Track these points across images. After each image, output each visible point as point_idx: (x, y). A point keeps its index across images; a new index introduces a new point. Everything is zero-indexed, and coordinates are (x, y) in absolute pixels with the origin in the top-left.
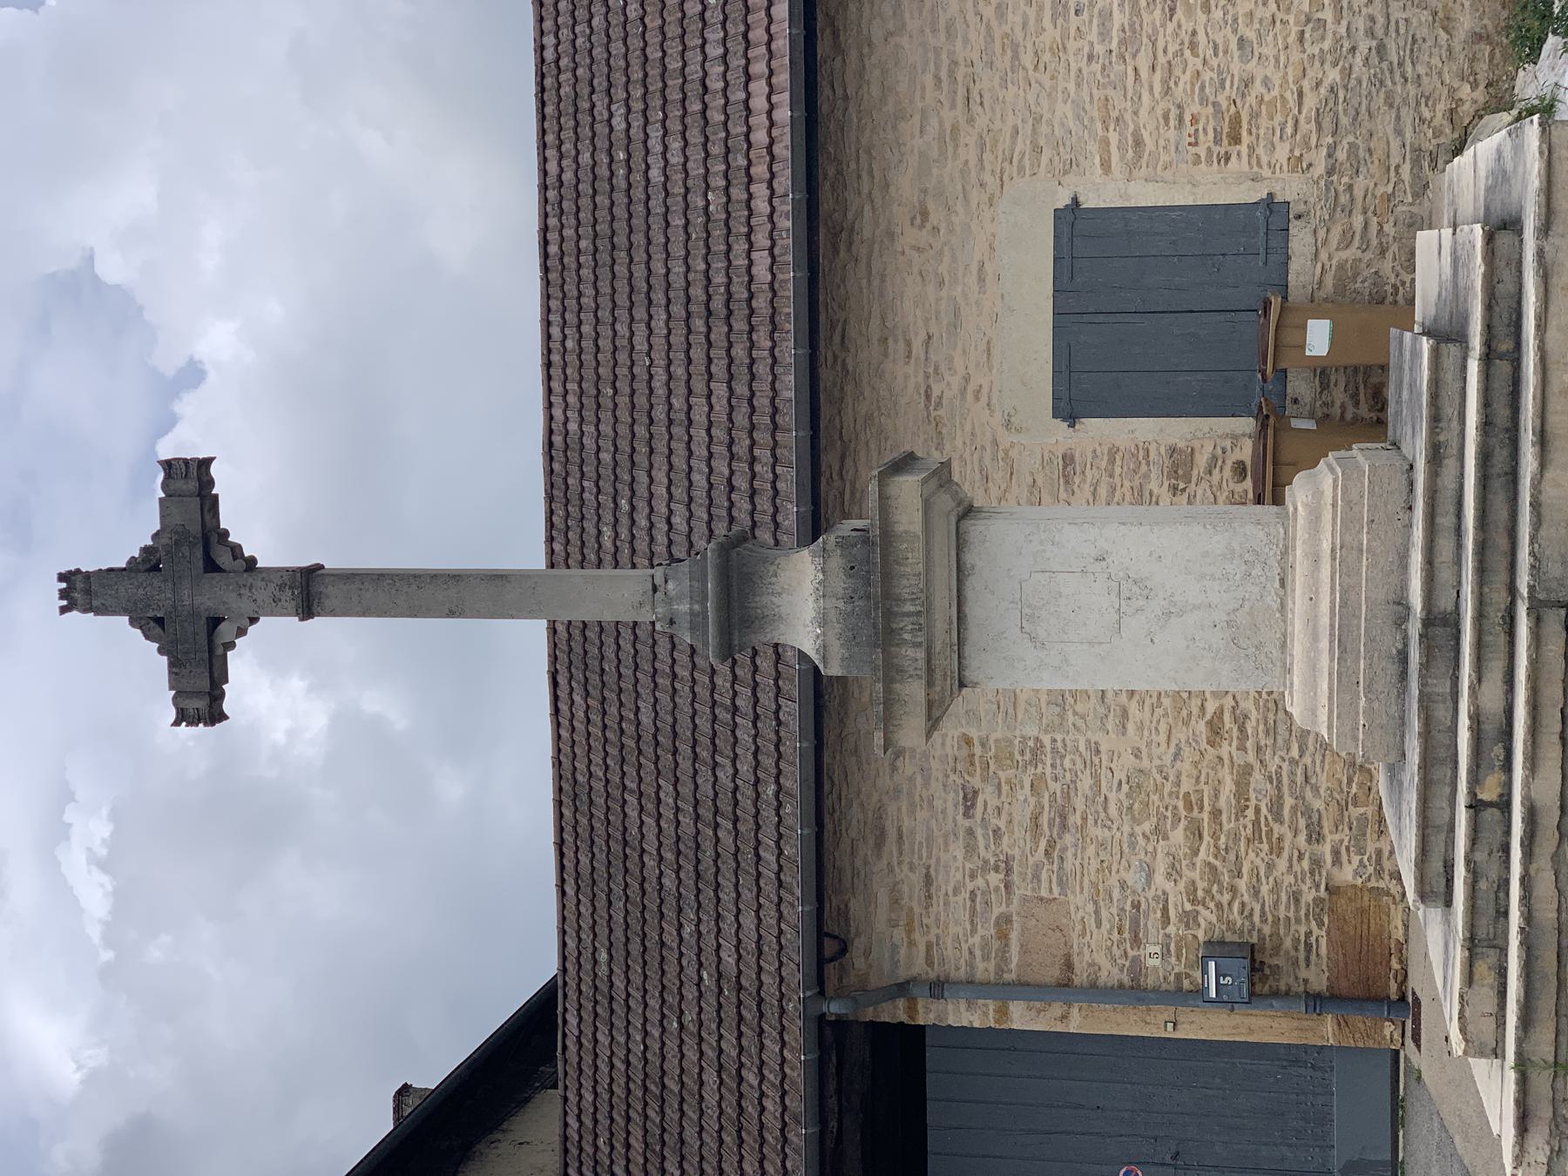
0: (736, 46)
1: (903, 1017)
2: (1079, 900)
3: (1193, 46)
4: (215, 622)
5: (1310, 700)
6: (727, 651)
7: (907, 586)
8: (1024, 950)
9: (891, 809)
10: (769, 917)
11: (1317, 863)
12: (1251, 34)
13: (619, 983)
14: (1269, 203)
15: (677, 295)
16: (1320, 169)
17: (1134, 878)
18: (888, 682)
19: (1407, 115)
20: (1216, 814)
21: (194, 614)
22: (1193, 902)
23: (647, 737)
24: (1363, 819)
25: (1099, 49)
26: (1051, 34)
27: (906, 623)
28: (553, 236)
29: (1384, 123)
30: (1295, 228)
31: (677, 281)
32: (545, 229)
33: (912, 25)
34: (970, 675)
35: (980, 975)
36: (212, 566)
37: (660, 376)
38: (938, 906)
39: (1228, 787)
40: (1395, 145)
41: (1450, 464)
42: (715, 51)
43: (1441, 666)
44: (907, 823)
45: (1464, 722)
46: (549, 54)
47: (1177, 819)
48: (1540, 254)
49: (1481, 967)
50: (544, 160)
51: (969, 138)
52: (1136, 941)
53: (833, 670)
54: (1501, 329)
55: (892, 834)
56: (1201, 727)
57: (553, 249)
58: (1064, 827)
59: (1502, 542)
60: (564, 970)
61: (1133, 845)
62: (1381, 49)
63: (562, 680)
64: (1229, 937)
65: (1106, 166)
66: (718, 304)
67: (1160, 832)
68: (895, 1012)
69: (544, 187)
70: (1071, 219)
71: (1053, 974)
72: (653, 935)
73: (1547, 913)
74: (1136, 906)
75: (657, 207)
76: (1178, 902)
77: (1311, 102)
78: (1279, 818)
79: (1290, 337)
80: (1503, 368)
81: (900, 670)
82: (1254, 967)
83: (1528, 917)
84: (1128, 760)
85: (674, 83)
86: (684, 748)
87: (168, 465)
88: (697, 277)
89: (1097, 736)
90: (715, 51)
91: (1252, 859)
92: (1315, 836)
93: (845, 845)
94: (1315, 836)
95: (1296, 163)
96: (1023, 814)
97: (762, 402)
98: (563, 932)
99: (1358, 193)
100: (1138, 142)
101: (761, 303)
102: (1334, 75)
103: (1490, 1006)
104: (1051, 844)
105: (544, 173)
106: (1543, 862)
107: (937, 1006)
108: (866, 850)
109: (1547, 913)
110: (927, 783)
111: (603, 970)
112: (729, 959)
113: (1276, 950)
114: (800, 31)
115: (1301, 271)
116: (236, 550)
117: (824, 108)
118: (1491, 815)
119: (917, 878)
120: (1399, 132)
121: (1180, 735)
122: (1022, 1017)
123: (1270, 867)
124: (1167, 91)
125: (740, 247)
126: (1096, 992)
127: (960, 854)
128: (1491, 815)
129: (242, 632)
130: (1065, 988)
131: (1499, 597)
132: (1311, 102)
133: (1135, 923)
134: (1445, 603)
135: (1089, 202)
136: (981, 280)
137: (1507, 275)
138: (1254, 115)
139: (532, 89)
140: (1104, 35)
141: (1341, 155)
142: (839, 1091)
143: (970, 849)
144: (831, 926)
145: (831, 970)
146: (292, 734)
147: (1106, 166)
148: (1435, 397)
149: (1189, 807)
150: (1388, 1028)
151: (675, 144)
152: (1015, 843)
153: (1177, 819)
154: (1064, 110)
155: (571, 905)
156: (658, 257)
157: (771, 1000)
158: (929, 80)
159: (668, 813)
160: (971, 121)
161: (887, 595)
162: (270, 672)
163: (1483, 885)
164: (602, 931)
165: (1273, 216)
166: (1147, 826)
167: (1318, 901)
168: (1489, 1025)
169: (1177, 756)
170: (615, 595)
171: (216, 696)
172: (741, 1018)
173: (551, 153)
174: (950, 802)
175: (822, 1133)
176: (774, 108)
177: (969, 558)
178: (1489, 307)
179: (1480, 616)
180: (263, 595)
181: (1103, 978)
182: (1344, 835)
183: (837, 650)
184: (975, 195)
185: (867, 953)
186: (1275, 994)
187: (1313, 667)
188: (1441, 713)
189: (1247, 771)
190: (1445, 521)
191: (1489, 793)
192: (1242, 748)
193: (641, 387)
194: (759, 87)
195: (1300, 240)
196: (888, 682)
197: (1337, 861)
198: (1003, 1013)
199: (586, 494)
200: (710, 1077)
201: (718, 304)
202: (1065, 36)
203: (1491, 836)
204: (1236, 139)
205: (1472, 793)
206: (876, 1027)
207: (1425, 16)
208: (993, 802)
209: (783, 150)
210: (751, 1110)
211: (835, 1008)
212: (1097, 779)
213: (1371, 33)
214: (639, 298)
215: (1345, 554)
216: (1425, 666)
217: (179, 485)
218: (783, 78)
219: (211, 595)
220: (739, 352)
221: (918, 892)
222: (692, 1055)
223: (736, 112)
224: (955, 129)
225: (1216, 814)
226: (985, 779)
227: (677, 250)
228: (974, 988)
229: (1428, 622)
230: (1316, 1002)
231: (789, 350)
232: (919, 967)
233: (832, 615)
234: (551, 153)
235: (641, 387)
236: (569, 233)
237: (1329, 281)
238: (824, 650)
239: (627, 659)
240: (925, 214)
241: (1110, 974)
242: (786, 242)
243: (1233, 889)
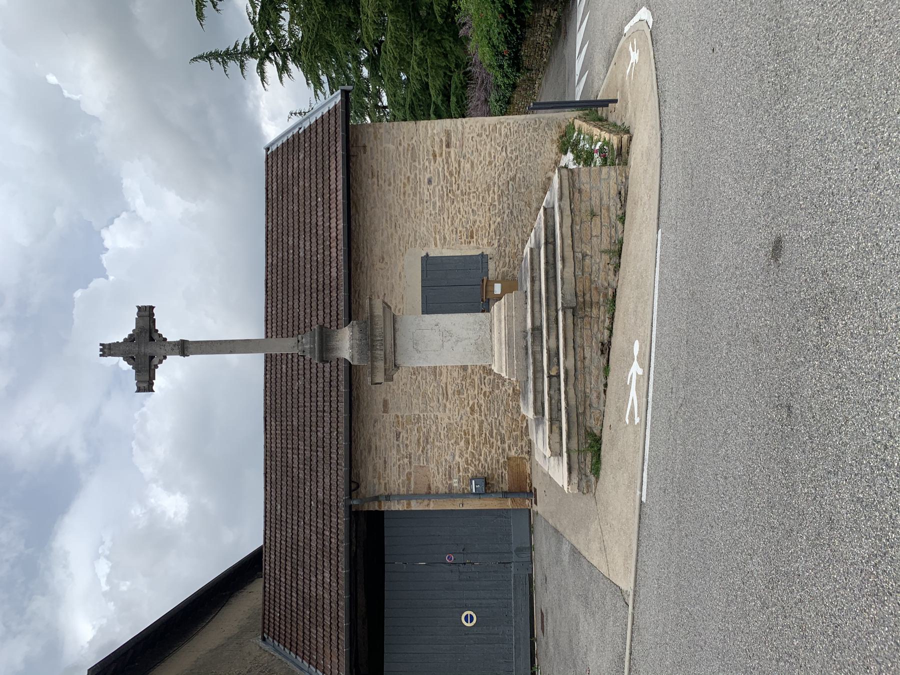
0: (326, 211)
1: (377, 508)
2: (432, 466)
3: (459, 212)
4: (152, 358)
5: (500, 366)
6: (323, 360)
7: (378, 331)
8: (415, 483)
9: (373, 440)
10: (334, 477)
11: (504, 450)
12: (475, 208)
13: (284, 515)
14: (482, 254)
15: (308, 288)
16: (496, 245)
17: (449, 458)
18: (372, 361)
19: (520, 231)
20: (473, 436)
21: (145, 354)
22: (467, 464)
23: (295, 428)
24: (517, 436)
25: (433, 212)
26: (419, 208)
27: (378, 343)
28: (269, 281)
29: (513, 233)
30: (490, 262)
31: (308, 284)
32: (267, 280)
33: (379, 206)
34: (398, 362)
35: (401, 493)
36: (152, 339)
37: (302, 313)
38: (388, 471)
39: (477, 427)
40: (517, 238)
41: (537, 282)
42: (320, 214)
43: (537, 343)
44: (378, 444)
45: (545, 351)
46: (270, 228)
47: (462, 438)
48: (560, 206)
49: (554, 427)
50: (267, 259)
51: (396, 237)
52: (450, 478)
53: (355, 363)
54: (549, 235)
55: (373, 447)
56: (468, 409)
57: (269, 285)
58: (427, 442)
59: (553, 297)
60: (265, 542)
61: (448, 447)
62: (512, 212)
63: (268, 419)
64: (479, 475)
65: (436, 245)
66: (320, 287)
67: (457, 443)
68: (374, 507)
69: (267, 267)
70: (426, 259)
71: (424, 490)
72: (295, 494)
73: (573, 402)
74: (450, 467)
75: (302, 264)
76: (462, 464)
77: (493, 227)
78: (492, 437)
79: (490, 288)
80: (550, 246)
81: (376, 358)
82: (487, 485)
83: (567, 404)
84: (446, 420)
85: (307, 226)
86: (308, 429)
87: (139, 308)
88: (314, 281)
89: (438, 413)
90: (320, 214)
91: (484, 450)
92: (503, 442)
93: (359, 452)
94: (503, 442)
95: (489, 244)
96: (414, 439)
97: (334, 313)
98: (266, 503)
99: (507, 252)
100: (445, 238)
101: (334, 284)
102: (499, 220)
103: (558, 440)
104: (424, 448)
105: (267, 263)
106: (571, 386)
107: (388, 503)
108: (365, 453)
109: (573, 402)
110: (384, 431)
111: (279, 512)
112: (320, 495)
113: (493, 478)
114: (346, 201)
115: (492, 274)
116: (160, 335)
117: (353, 228)
118: (554, 379)
119: (382, 462)
120: (518, 235)
121: (462, 412)
122: (415, 506)
123: (490, 452)
124: (452, 224)
125: (327, 269)
126: (438, 496)
127: (395, 453)
128: (554, 379)
129: (161, 362)
130: (429, 494)
131: (553, 313)
132: (493, 227)
133: (450, 472)
134: (537, 324)
135: (431, 255)
136: (400, 278)
137: (550, 220)
138: (477, 231)
139: (264, 239)
140: (434, 209)
141: (502, 242)
142: (356, 537)
143: (398, 451)
144: (354, 479)
145: (354, 494)
146: (176, 514)
147: (436, 245)
148: (532, 263)
149: (465, 434)
150: (527, 502)
151: (308, 244)
152: (413, 448)
153: (462, 438)
154: (423, 229)
155: (269, 493)
156: (302, 278)
157: (334, 504)
158: (384, 220)
159: (301, 452)
160: (396, 232)
161: (372, 335)
162: (170, 372)
163: (553, 401)
164: (279, 499)
165: (483, 259)
166: (453, 441)
167: (505, 462)
168: (558, 445)
169: (461, 418)
170: (286, 346)
171: (151, 384)
172: (324, 514)
173: (270, 257)
174: (391, 436)
175: (350, 546)
176: (338, 225)
177: (397, 326)
178: (546, 229)
179: (548, 319)
180: (168, 348)
181: (440, 491)
182: (511, 441)
183: (356, 356)
184: (398, 253)
185: (366, 488)
186: (492, 492)
187: (500, 353)
188: (538, 356)
189: (482, 422)
190: (537, 299)
191: (553, 373)
192: (481, 415)
193: (296, 319)
194: (333, 221)
195: (491, 265)
196: (372, 361)
197: (510, 449)
198: (409, 504)
199: (277, 319)
200: (314, 538)
201: (320, 287)
202: (423, 209)
203: (555, 386)
204: (472, 237)
205: (548, 373)
206: (369, 512)
207: (523, 203)
208: (405, 436)
209: (340, 237)
210: (327, 544)
211: (355, 502)
212: (437, 426)
213: (508, 208)
214: (296, 292)
215: (509, 318)
216: (533, 342)
217: (143, 313)
218: (341, 216)
219: (150, 349)
220: (327, 300)
221: (382, 466)
222: (307, 532)
223: (326, 229)
224: (392, 234)
225: (473, 436)
226: (403, 428)
227: (308, 275)
228: (400, 497)
229: (533, 329)
230: (505, 494)
231: (342, 294)
232: (382, 491)
233: (355, 345)
234: (270, 257)
235: (296, 319)
236: (274, 279)
237: (500, 277)
238: (352, 357)
239: (289, 405)
240: (383, 259)
241: (443, 489)
242: (341, 263)
243: (479, 460)
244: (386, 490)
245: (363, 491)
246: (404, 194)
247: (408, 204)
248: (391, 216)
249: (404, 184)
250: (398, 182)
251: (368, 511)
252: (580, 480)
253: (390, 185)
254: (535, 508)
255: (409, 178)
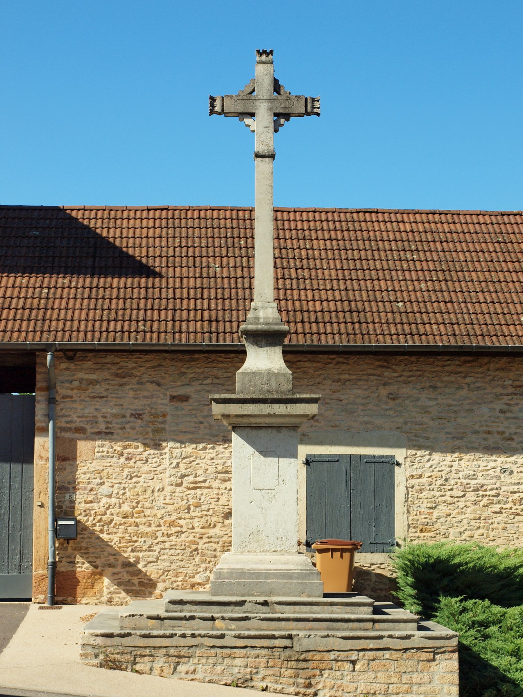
25: (461, 475)
89: (168, 474)
127: (114, 411)
143: (115, 416)
145: (61, 354)
177: (284, 431)
185: (67, 369)
215: (287, 575)
244: (63, 397)
245: (63, 366)
246: (489, 433)
247: (473, 437)
248: (455, 412)
249: (503, 433)
250: (506, 423)
251: (35, 371)
252: (94, 647)
253: (502, 411)
254: (33, 607)
255: (512, 439)
